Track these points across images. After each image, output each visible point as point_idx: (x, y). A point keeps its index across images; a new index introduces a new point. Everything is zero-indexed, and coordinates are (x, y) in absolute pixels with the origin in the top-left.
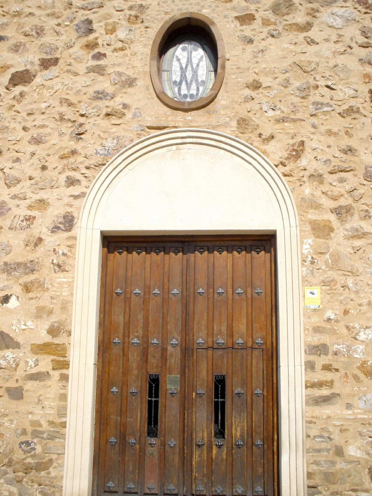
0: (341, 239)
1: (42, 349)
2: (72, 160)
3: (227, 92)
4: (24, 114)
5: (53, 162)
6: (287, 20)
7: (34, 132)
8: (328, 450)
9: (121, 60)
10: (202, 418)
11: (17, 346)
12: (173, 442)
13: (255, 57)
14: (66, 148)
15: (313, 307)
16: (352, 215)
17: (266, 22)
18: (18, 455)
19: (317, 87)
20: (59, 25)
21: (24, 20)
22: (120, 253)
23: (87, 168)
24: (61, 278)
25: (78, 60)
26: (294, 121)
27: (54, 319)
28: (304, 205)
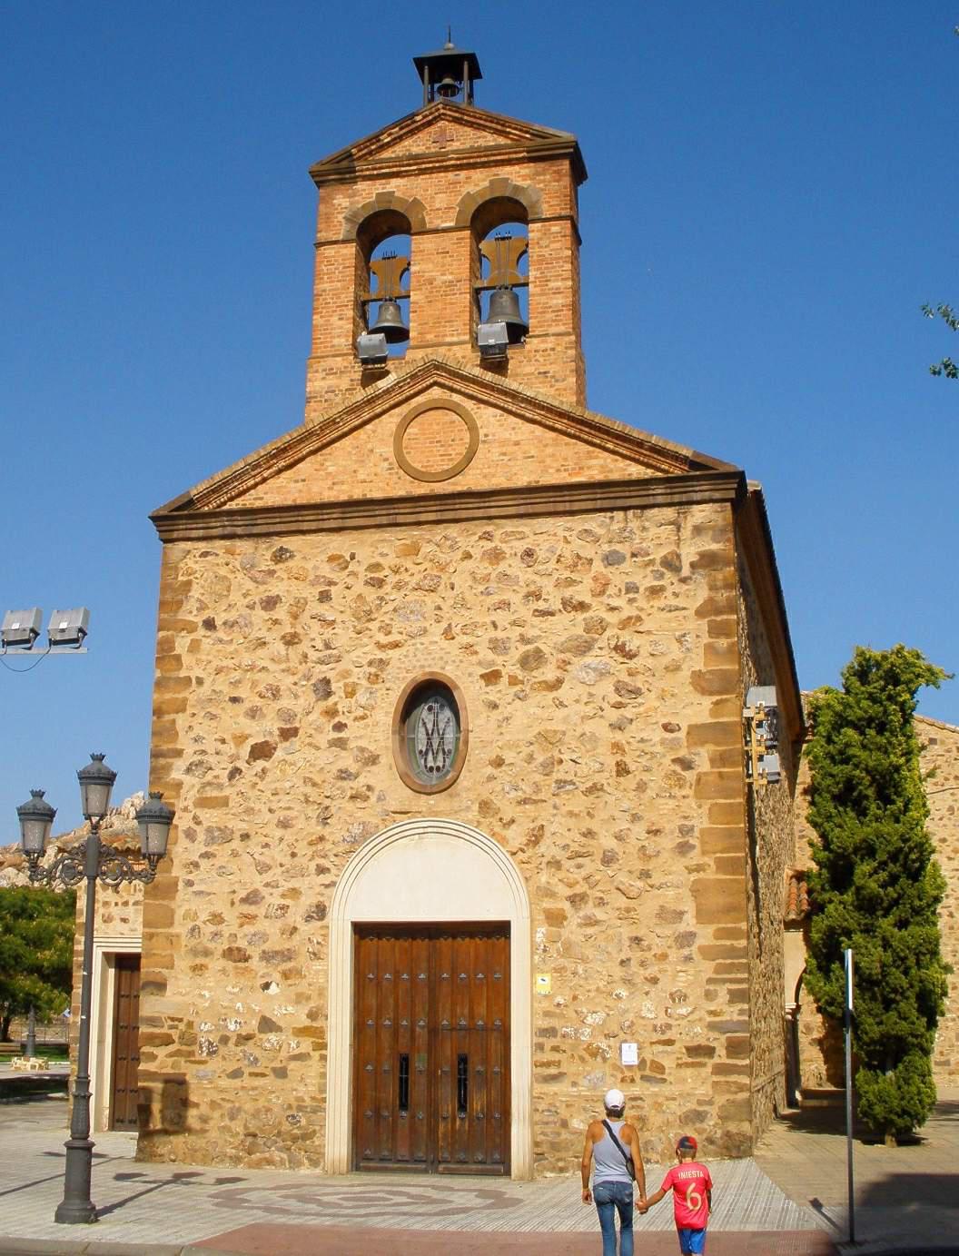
0: (574, 927)
1: (302, 1032)
2: (320, 847)
3: (470, 771)
4: (268, 794)
5: (302, 848)
7: (281, 815)
8: (555, 1123)
9: (362, 732)
10: (447, 1093)
11: (279, 1029)
12: (421, 1115)
13: (499, 726)
14: (313, 834)
15: (543, 993)
16: (586, 903)
17: (513, 681)
18: (286, 1127)
19: (561, 762)
20: (295, 684)
21: (258, 676)
22: (371, 940)
23: (336, 855)
24: (317, 965)
25: (319, 729)
26: (535, 802)
27: (312, 1004)
28: (540, 893)
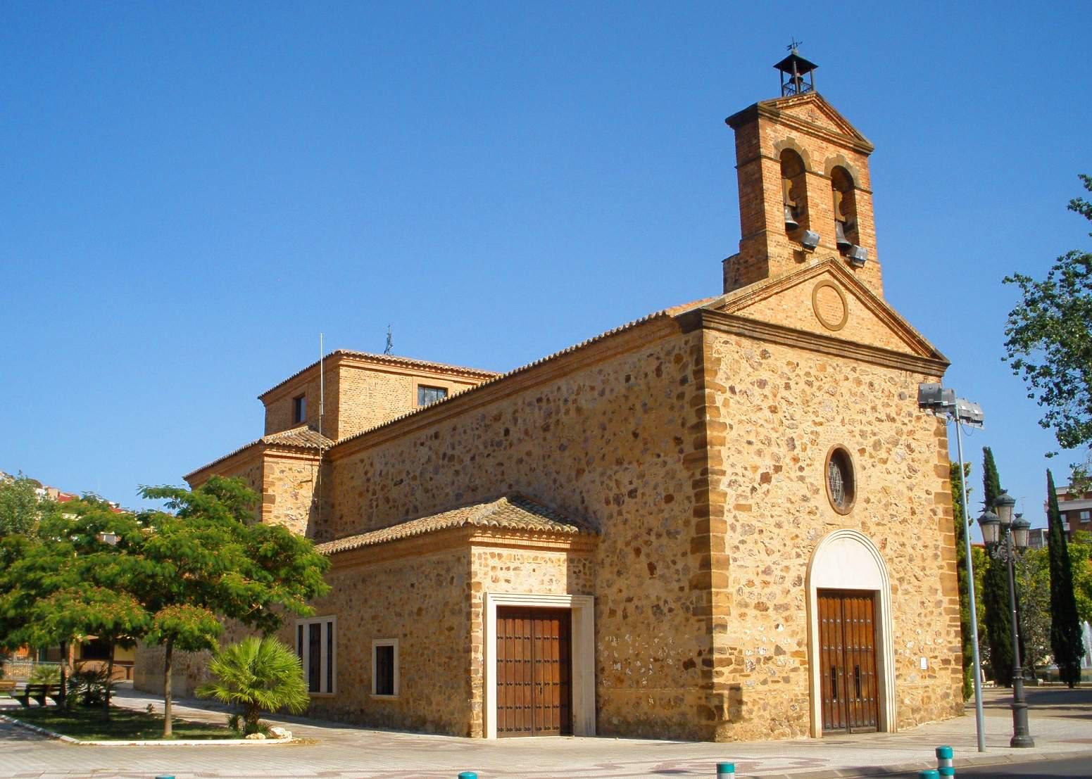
6: (970, 525)
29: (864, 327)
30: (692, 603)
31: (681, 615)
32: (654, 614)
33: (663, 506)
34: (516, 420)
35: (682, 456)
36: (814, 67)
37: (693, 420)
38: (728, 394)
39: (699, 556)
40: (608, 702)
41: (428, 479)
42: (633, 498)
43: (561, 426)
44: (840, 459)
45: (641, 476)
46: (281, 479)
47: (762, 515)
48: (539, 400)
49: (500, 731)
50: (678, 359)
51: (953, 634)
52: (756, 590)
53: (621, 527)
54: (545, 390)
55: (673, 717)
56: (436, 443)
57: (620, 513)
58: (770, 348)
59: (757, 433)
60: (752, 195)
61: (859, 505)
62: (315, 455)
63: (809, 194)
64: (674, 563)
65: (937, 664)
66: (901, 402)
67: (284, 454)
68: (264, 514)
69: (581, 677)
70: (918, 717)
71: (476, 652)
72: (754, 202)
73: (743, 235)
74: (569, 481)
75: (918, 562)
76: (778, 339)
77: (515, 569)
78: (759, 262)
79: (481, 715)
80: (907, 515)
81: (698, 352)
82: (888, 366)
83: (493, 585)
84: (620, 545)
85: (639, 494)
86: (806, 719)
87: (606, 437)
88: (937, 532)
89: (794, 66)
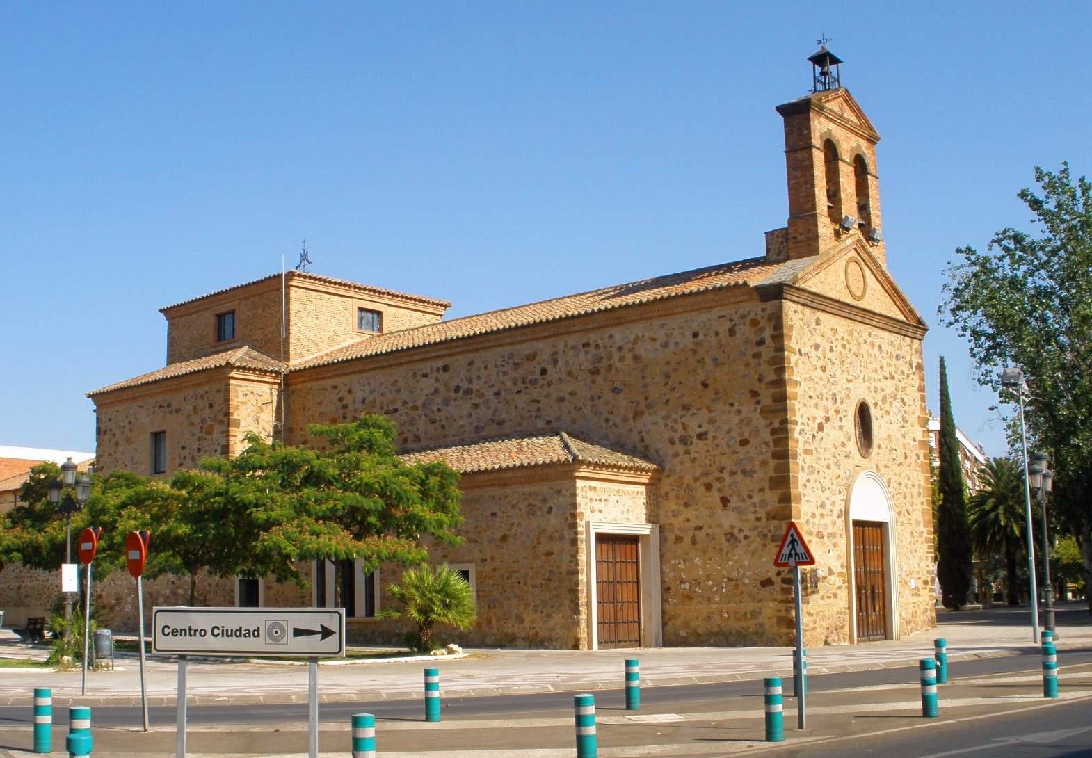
29: (878, 301)
30: (770, 531)
31: (757, 543)
32: (728, 540)
33: (738, 448)
34: (555, 362)
35: (759, 407)
36: (840, 62)
37: (770, 376)
38: (798, 355)
39: (778, 493)
40: (674, 617)
41: (435, 410)
42: (702, 439)
43: (613, 371)
44: (863, 413)
45: (712, 421)
46: (244, 403)
47: (819, 459)
48: (586, 345)
49: (602, 643)
50: (754, 323)
51: (929, 559)
52: (817, 520)
53: (688, 464)
54: (594, 337)
55: (749, 628)
56: (447, 375)
57: (687, 452)
58: (821, 315)
59: (815, 389)
60: (802, 179)
61: (874, 450)
62: (275, 378)
63: (841, 180)
64: (750, 497)
65: (920, 585)
66: (898, 362)
67: (248, 377)
68: (230, 439)
69: (651, 596)
70: (909, 627)
71: (582, 574)
72: (804, 187)
73: (791, 214)
74: (625, 420)
75: (909, 499)
76: (828, 309)
77: (605, 501)
78: (809, 239)
79: (586, 630)
80: (902, 459)
81: (777, 321)
82: (890, 331)
83: (591, 514)
84: (688, 479)
85: (710, 436)
86: (847, 629)
87: (670, 384)
88: (920, 473)
89: (823, 59)
